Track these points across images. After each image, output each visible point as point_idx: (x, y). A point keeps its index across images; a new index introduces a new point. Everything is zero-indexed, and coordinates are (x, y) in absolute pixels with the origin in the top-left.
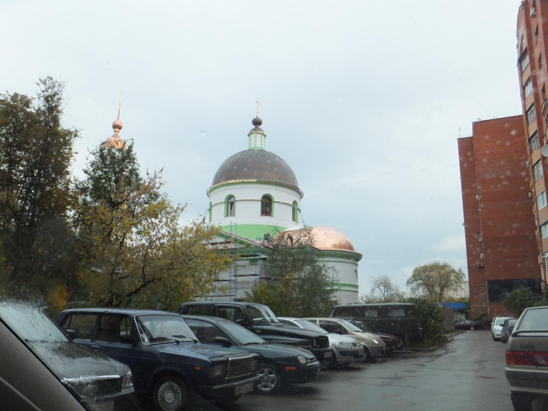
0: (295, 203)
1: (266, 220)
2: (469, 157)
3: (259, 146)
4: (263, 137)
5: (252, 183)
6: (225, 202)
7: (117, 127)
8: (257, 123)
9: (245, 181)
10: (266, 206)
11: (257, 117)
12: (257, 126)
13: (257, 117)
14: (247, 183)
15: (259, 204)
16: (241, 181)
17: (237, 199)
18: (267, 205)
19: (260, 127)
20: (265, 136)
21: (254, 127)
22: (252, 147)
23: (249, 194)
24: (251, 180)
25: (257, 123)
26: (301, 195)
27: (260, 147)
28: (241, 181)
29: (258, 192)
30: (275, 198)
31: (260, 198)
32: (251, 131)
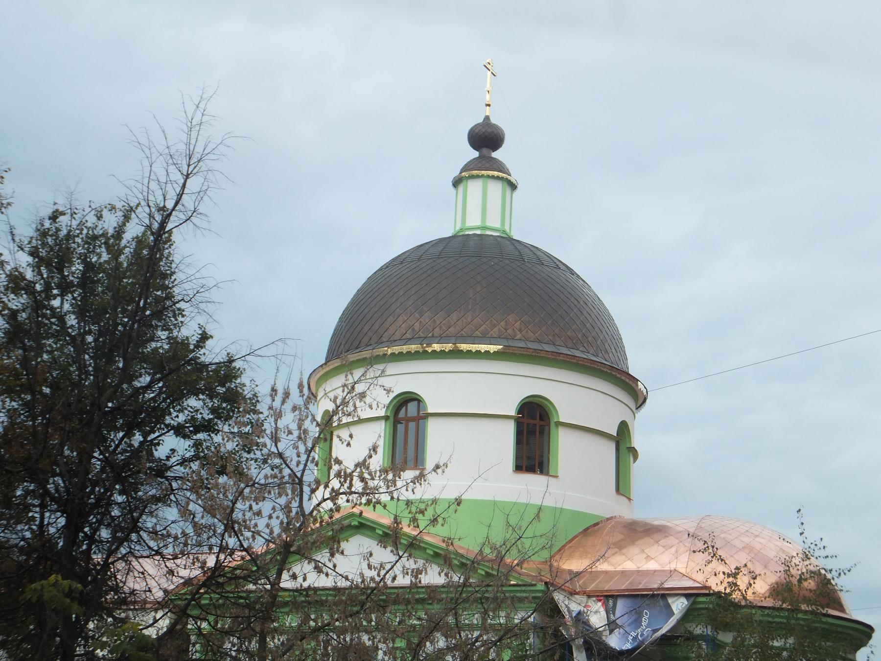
0: (624, 428)
1: (531, 488)
2: (466, 580)
3: (494, 222)
4: (508, 190)
5: (487, 355)
6: (386, 418)
7: (55, 204)
8: (486, 139)
9: (464, 347)
10: (531, 432)
11: (487, 118)
12: (485, 151)
13: (487, 118)
14: (469, 355)
15: (509, 430)
16: (448, 347)
17: (430, 410)
18: (534, 429)
19: (495, 155)
20: (513, 186)
21: (476, 154)
22: (468, 224)
23: (470, 395)
24: (483, 348)
25: (486, 139)
26: (639, 399)
27: (498, 225)
28: (413, 348)
29: (505, 386)
30: (564, 412)
31: (513, 412)
32: (465, 169)
